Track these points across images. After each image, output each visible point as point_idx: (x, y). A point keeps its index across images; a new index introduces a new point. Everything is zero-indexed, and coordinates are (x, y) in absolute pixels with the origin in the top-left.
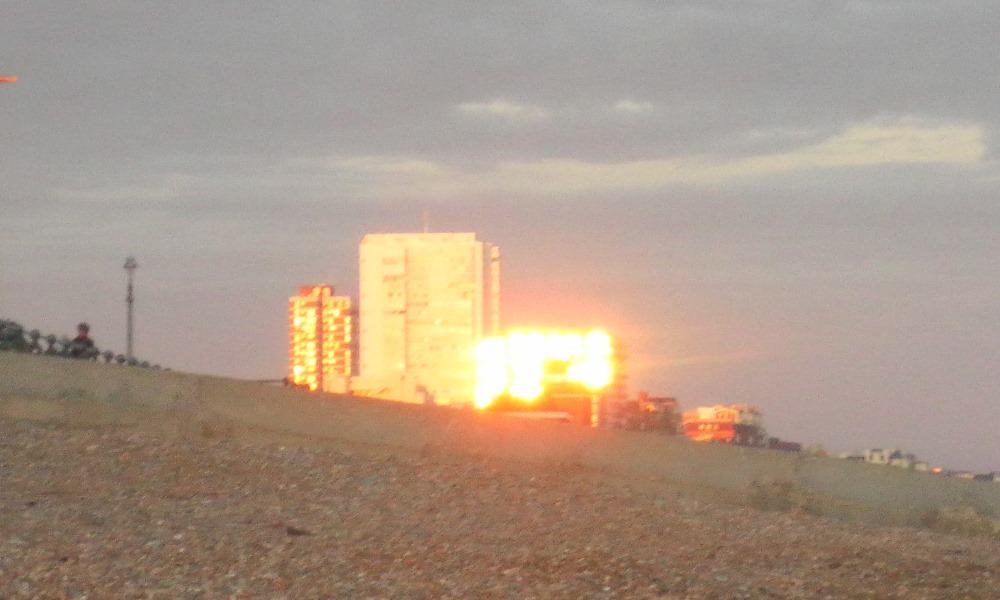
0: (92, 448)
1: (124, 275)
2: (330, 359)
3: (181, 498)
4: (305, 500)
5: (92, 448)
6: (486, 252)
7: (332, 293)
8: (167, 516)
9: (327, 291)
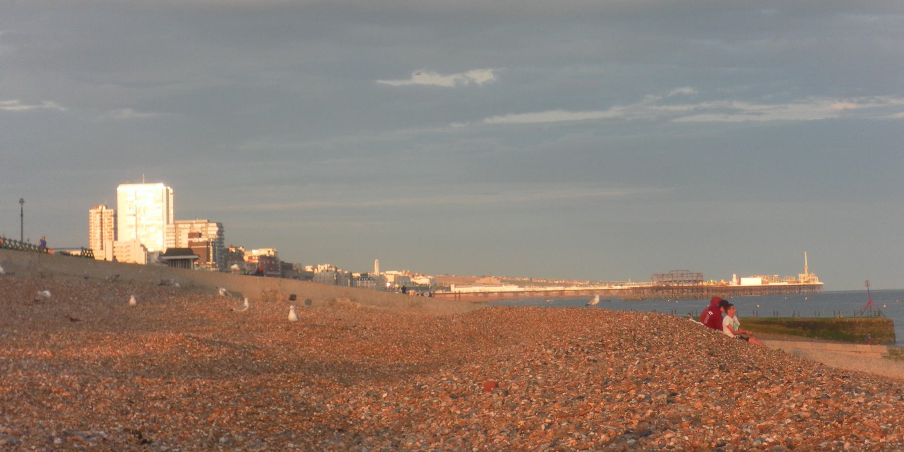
1: (19, 206)
2: (106, 234)
3: (30, 305)
6: (167, 191)
7: (107, 208)
8: (23, 313)
9: (104, 207)
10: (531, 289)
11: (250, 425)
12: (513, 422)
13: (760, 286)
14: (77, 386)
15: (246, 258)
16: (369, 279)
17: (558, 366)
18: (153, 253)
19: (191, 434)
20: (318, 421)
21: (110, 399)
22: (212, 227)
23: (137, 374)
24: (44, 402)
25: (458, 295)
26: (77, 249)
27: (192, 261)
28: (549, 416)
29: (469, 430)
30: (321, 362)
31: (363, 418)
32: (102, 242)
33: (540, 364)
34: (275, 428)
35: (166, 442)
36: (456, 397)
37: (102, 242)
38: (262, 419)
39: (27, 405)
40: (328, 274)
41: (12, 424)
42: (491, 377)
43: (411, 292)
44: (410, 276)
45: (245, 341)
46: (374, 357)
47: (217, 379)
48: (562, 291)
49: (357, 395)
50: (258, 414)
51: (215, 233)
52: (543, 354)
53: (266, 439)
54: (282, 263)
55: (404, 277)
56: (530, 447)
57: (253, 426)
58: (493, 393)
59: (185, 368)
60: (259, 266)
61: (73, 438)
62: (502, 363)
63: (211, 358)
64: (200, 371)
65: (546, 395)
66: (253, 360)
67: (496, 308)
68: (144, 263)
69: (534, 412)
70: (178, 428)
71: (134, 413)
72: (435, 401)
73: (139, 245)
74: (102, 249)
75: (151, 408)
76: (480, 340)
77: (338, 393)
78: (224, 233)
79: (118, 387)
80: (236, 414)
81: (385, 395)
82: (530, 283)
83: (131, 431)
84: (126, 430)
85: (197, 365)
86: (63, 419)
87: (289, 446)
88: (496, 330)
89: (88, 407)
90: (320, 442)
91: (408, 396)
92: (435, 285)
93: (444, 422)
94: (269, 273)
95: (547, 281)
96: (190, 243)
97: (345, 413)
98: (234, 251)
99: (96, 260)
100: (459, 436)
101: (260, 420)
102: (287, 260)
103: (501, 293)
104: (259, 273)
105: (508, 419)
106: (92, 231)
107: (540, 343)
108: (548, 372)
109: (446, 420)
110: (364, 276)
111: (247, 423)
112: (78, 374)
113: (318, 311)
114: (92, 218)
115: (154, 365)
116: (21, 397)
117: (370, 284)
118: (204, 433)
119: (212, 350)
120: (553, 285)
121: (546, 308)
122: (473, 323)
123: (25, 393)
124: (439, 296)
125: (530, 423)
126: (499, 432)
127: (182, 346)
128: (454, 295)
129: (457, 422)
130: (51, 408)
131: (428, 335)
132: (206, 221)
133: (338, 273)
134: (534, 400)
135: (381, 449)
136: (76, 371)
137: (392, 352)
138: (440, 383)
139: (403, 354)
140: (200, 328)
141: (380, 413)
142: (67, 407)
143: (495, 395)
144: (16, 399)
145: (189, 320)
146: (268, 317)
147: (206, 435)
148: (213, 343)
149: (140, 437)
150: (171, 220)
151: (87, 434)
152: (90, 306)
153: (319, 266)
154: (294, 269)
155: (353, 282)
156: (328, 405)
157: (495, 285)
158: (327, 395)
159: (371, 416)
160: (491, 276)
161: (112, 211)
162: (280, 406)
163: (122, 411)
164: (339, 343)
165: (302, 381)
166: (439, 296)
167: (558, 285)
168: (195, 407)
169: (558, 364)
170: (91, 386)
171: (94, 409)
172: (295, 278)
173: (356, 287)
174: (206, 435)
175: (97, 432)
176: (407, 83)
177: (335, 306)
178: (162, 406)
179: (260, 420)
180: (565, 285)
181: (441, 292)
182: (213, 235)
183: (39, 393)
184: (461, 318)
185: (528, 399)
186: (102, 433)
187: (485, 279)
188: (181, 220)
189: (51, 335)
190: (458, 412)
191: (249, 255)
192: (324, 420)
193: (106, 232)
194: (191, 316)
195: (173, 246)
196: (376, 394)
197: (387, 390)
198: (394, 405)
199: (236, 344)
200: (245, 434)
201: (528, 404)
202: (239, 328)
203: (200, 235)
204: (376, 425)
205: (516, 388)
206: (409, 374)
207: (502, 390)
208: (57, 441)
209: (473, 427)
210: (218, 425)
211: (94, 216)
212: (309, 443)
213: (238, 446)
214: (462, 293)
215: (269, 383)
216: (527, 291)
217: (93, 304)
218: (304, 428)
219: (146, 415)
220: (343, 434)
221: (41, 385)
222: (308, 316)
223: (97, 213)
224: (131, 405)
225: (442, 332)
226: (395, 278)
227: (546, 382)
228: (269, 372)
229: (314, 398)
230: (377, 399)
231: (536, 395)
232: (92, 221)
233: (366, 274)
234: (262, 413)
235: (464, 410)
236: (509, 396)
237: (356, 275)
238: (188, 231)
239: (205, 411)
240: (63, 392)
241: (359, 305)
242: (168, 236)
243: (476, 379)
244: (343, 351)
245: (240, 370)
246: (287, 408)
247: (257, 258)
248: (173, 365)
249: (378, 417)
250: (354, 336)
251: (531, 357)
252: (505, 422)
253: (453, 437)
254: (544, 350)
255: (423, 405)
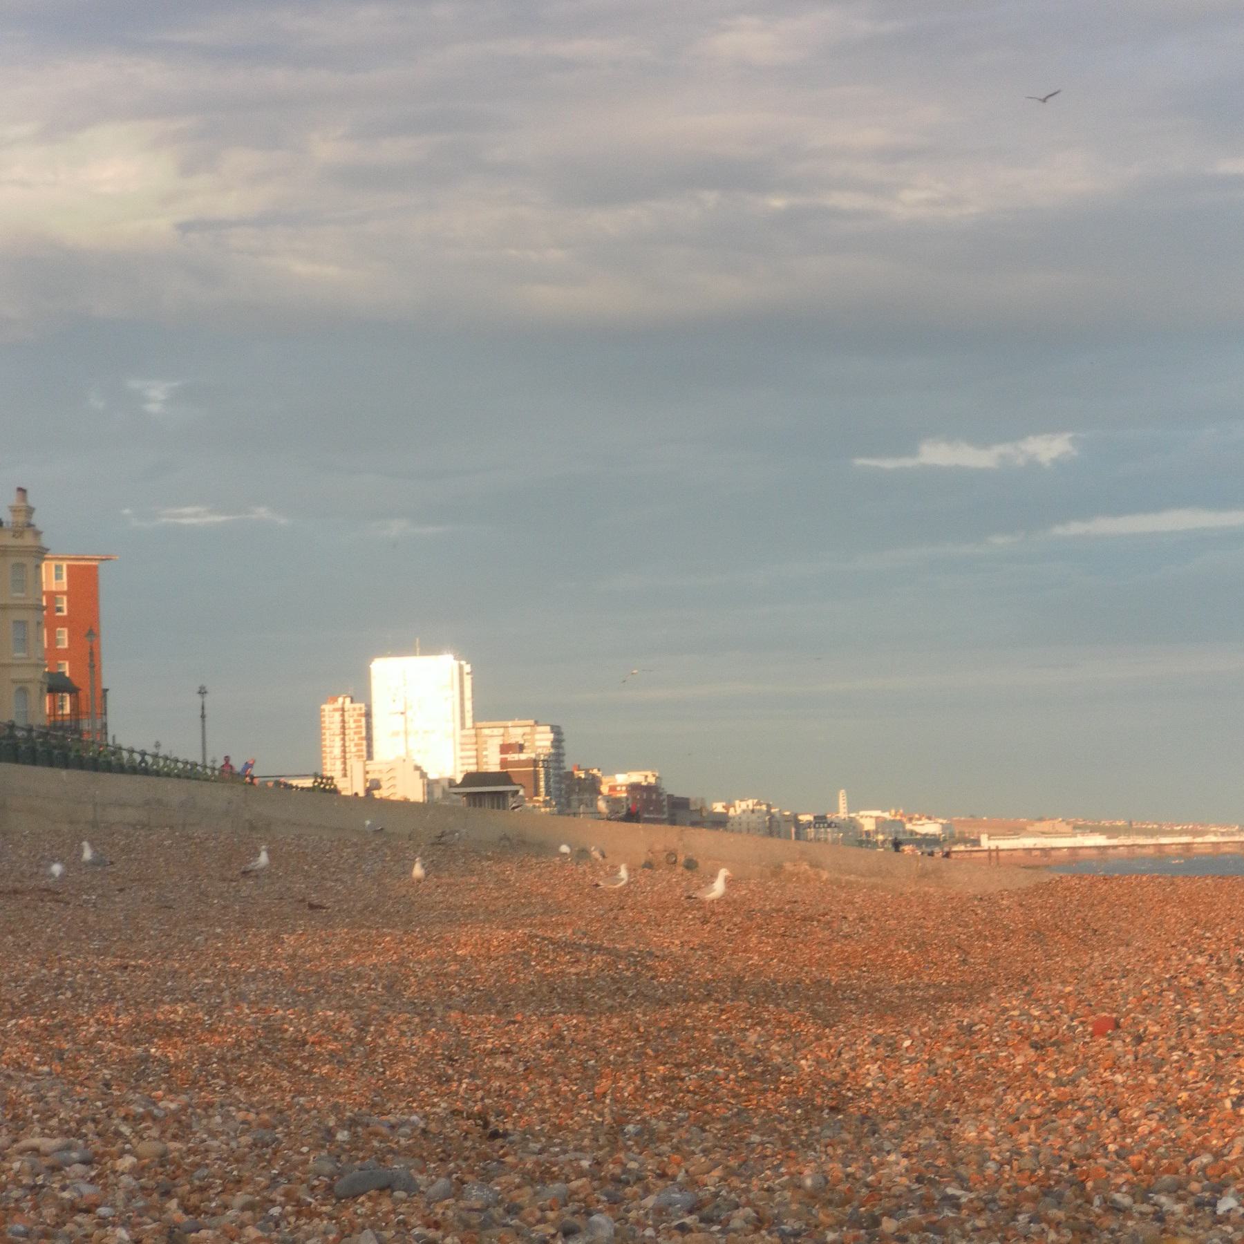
0: (167, 843)
1: (198, 699)
2: (352, 748)
3: (232, 881)
4: (323, 878)
5: (167, 843)
6: (461, 667)
7: (352, 702)
8: (221, 896)
9: (348, 700)
10: (1129, 842)
11: (673, 1101)
12: (1165, 1093)
13: (499, 773)
14: (351, 1031)
15: (605, 789)
16: (829, 826)
17: (1226, 988)
18: (437, 782)
19: (572, 1119)
20: (791, 1092)
21: (414, 1054)
22: (543, 733)
23: (450, 1007)
24: (298, 1062)
25: (994, 854)
26: (305, 776)
27: (510, 794)
28: (1234, 1081)
29: (1082, 1109)
30: (774, 982)
31: (869, 1085)
32: (344, 763)
33: (1191, 984)
34: (718, 1105)
35: (532, 1135)
36: (1042, 1047)
37: (344, 763)
38: (691, 1088)
39: (268, 1068)
40: (754, 817)
41: (252, 1105)
42: (1104, 1011)
43: (907, 849)
44: (905, 820)
45: (632, 944)
46: (868, 971)
47: (594, 1015)
48: (1188, 844)
49: (855, 1043)
50: (682, 1079)
51: (548, 743)
52: (1189, 965)
53: (707, 1127)
54: (670, 796)
55: (893, 821)
56: (1214, 1142)
57: (677, 1103)
58: (1112, 1039)
59: (533, 993)
60: (630, 802)
61: (370, 1129)
62: (1115, 982)
63: (577, 974)
64: (562, 1000)
65: (1217, 1043)
66: (652, 978)
67: (1080, 878)
68: (421, 801)
69: (1201, 1076)
70: (547, 1106)
71: (460, 1082)
72: (1004, 1054)
73: (412, 768)
74: (345, 775)
75: (489, 1069)
76: (1056, 939)
77: (818, 1038)
78: (564, 744)
79: (424, 1031)
80: (643, 1080)
81: (907, 1043)
82: (1128, 830)
83: (465, 1115)
84: (455, 1113)
85: (554, 989)
86: (340, 1094)
87: (752, 1139)
88: (1084, 920)
89: (376, 1071)
90: (806, 1132)
91: (950, 1045)
92: (952, 836)
93: (1028, 1095)
94: (647, 816)
95: (1160, 825)
96: (504, 763)
97: (836, 1076)
98: (583, 776)
99: (346, 797)
100: (1065, 1121)
101: (689, 1092)
102: (678, 793)
103: (1073, 849)
104: (632, 817)
105: (1154, 1088)
106: (327, 743)
107: (1174, 943)
108: (1210, 999)
109: (1032, 1090)
110: (820, 820)
111: (666, 1096)
112: (348, 1008)
113: (751, 886)
114: (327, 719)
115: (478, 990)
116: (254, 1052)
117: (831, 834)
118: (595, 1116)
119: (577, 961)
120: (1171, 833)
121: (1172, 877)
122: (1041, 908)
123: (260, 1047)
124: (959, 856)
125: (1199, 1097)
126: (1144, 1114)
127: (524, 953)
128: (985, 854)
129: (1053, 1094)
130: (309, 1072)
131: (960, 929)
132: (531, 722)
133: (772, 816)
134: (1197, 1053)
135: (920, 1145)
136: (343, 1002)
137: (900, 961)
138: (1007, 1020)
139: (919, 965)
140: (546, 919)
141: (900, 1076)
142: (339, 1071)
143: (1117, 1044)
144: (246, 1057)
145: (523, 904)
146: (663, 899)
147: (600, 1119)
148: (579, 948)
149: (486, 1125)
150: (469, 723)
151: (389, 1121)
152: (343, 882)
153: (737, 802)
154: (692, 808)
155: (801, 831)
156: (803, 1062)
157: (1058, 834)
158: (799, 1044)
159: (884, 1082)
160: (1056, 819)
161: (363, 705)
162: (718, 1064)
163: (439, 1077)
164: (800, 945)
165: (748, 1018)
166: (959, 856)
167: (1181, 833)
168: (568, 1068)
169: (1225, 984)
170: (376, 1031)
171: (388, 1073)
172: (694, 824)
173: (806, 840)
174: (600, 1119)
175: (406, 1117)
176: (908, 462)
177: (782, 877)
178: (508, 1065)
179: (689, 1092)
180: (1195, 833)
181: (962, 848)
182: (544, 747)
183: (285, 1046)
184: (1016, 898)
185: (1185, 1050)
186: (414, 1118)
187: (1044, 824)
188: (487, 721)
189: (285, 936)
190: (1052, 1075)
191: (611, 784)
192: (801, 1089)
193: (352, 745)
194: (525, 897)
195: (473, 768)
196: (891, 1041)
197: (909, 1034)
198: (926, 1062)
199: (618, 950)
200: (667, 1117)
201: (1186, 1060)
202: (616, 918)
203: (521, 748)
204: (895, 1098)
205: (1156, 1029)
206: (936, 1002)
207: (1129, 1033)
208: (342, 1136)
209: (1088, 1104)
210: (615, 1100)
211: (330, 716)
212: (785, 1133)
213: (662, 1140)
214: (1003, 850)
215: (688, 1021)
216: (1123, 846)
217: (346, 877)
218: (770, 1106)
219: (484, 1085)
220: (840, 1117)
221: (287, 1030)
222: (735, 896)
223: (335, 710)
224: (452, 1065)
225: (986, 924)
226: (877, 824)
227: (1211, 1017)
228: (687, 1001)
229: (775, 1048)
230: (892, 1051)
231: (1197, 1042)
232: (326, 725)
233: (824, 817)
234: (691, 1080)
235: (1063, 1071)
236: (1145, 1044)
237: (805, 818)
238: (499, 741)
239: (588, 1077)
240: (328, 1042)
241: (825, 875)
242: (462, 750)
243: (1074, 1013)
244: (810, 960)
245: (633, 997)
246: (733, 1068)
247: (624, 788)
248: (513, 989)
249: (897, 1085)
250: (827, 933)
251: (1168, 971)
252: (1149, 1094)
253: (1053, 1121)
254: (1190, 957)
255: (980, 1062)
